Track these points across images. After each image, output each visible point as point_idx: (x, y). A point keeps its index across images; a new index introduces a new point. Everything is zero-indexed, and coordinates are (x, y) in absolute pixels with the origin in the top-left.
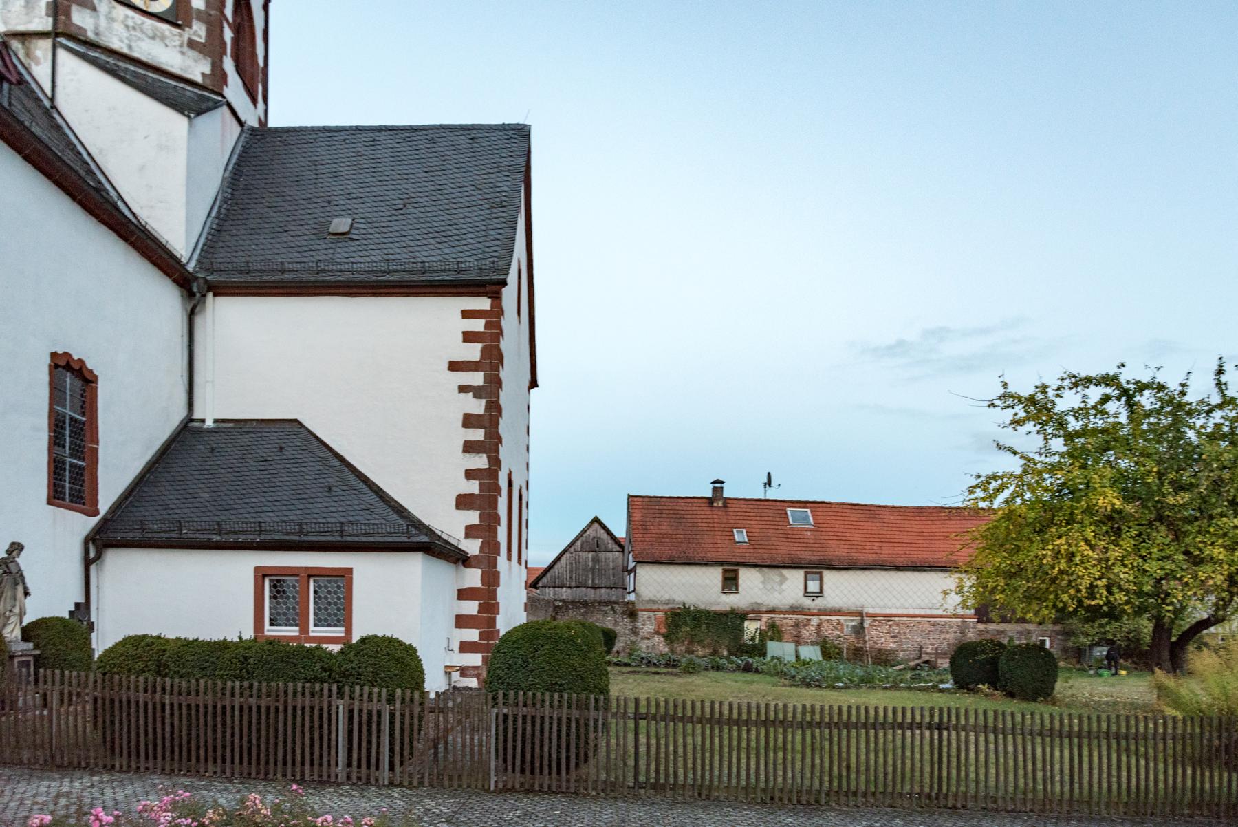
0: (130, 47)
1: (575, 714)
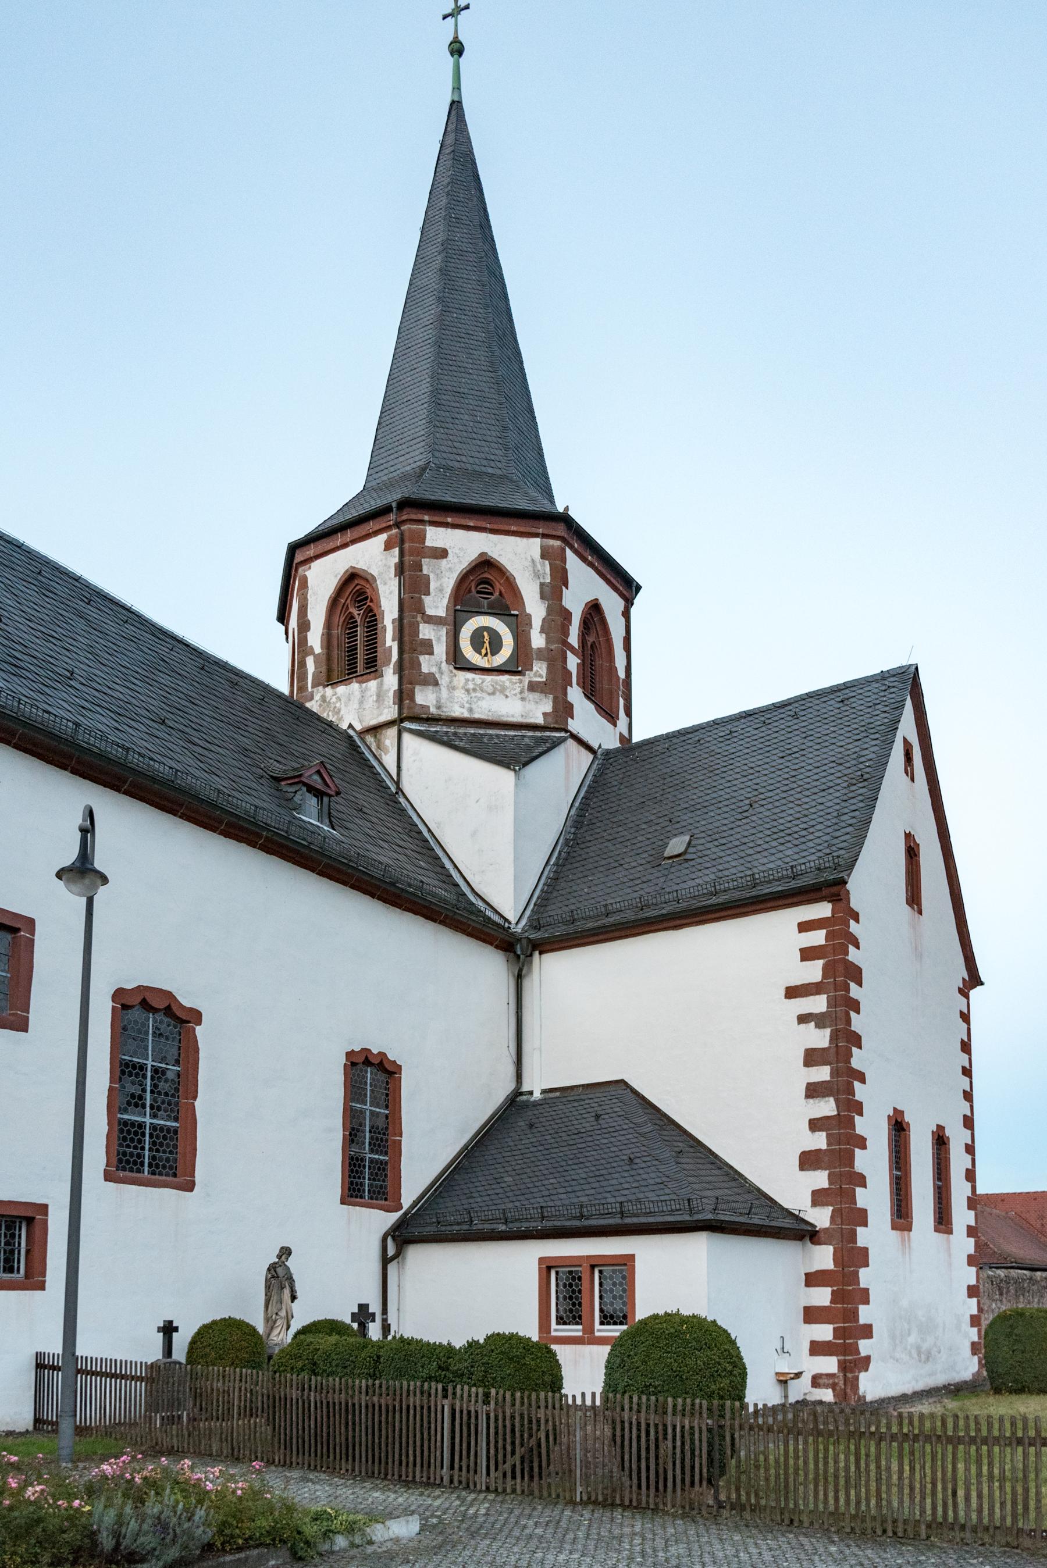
0: (471, 710)
1: (653, 1419)
